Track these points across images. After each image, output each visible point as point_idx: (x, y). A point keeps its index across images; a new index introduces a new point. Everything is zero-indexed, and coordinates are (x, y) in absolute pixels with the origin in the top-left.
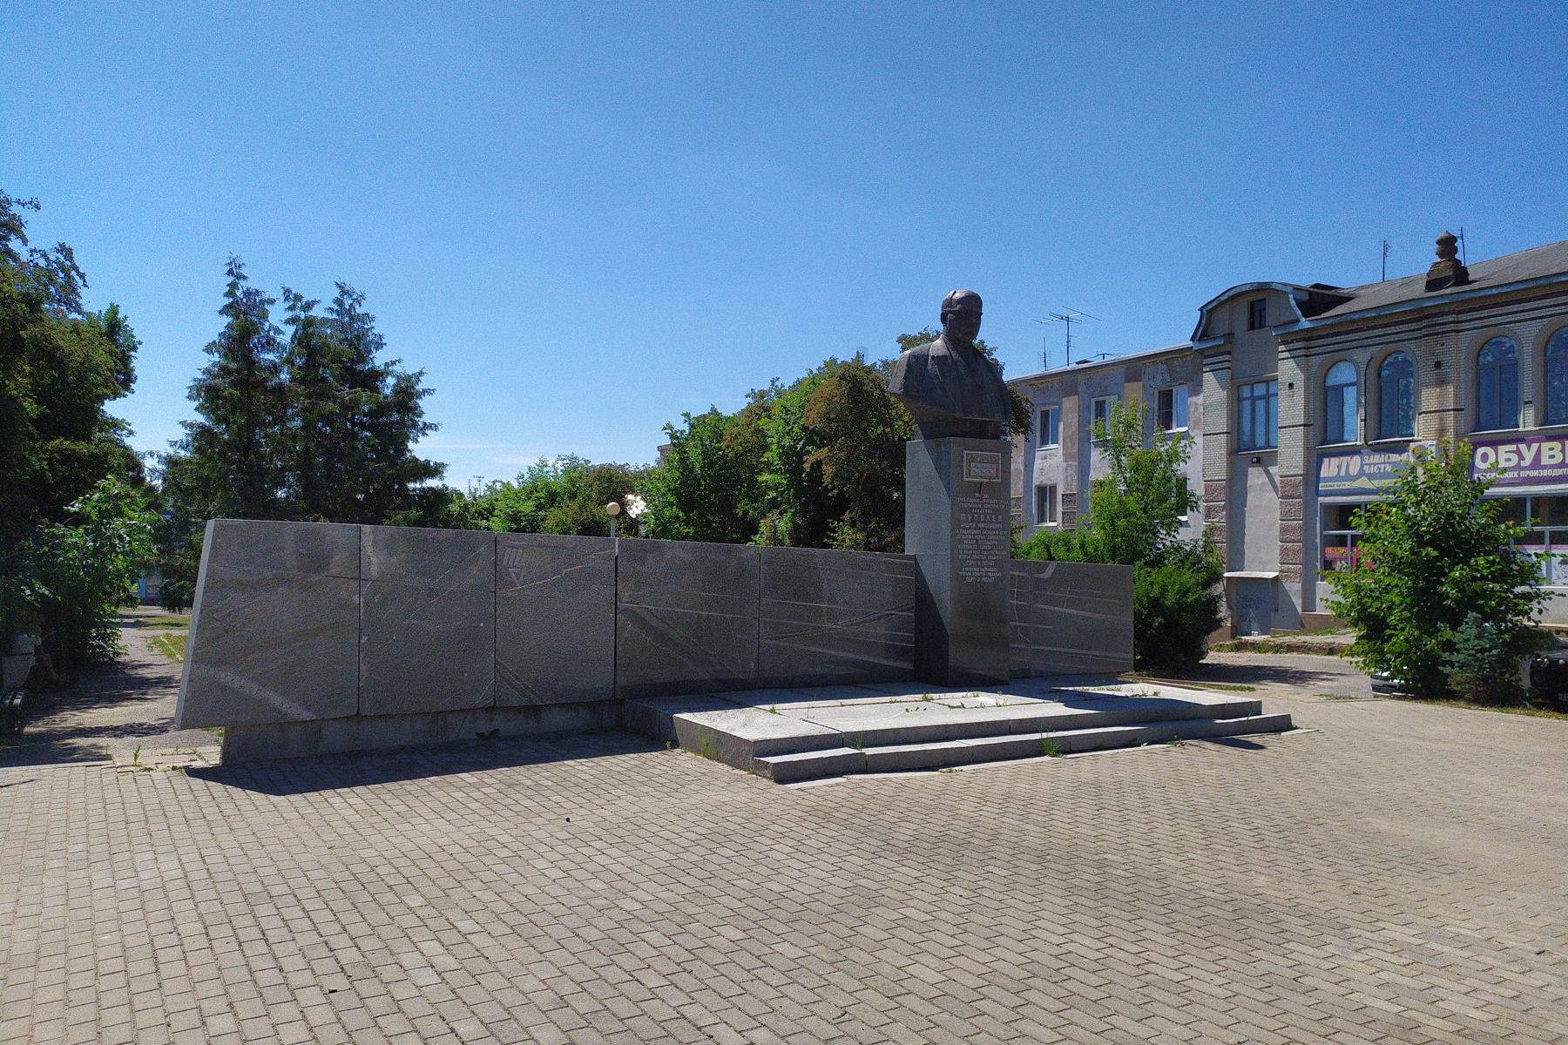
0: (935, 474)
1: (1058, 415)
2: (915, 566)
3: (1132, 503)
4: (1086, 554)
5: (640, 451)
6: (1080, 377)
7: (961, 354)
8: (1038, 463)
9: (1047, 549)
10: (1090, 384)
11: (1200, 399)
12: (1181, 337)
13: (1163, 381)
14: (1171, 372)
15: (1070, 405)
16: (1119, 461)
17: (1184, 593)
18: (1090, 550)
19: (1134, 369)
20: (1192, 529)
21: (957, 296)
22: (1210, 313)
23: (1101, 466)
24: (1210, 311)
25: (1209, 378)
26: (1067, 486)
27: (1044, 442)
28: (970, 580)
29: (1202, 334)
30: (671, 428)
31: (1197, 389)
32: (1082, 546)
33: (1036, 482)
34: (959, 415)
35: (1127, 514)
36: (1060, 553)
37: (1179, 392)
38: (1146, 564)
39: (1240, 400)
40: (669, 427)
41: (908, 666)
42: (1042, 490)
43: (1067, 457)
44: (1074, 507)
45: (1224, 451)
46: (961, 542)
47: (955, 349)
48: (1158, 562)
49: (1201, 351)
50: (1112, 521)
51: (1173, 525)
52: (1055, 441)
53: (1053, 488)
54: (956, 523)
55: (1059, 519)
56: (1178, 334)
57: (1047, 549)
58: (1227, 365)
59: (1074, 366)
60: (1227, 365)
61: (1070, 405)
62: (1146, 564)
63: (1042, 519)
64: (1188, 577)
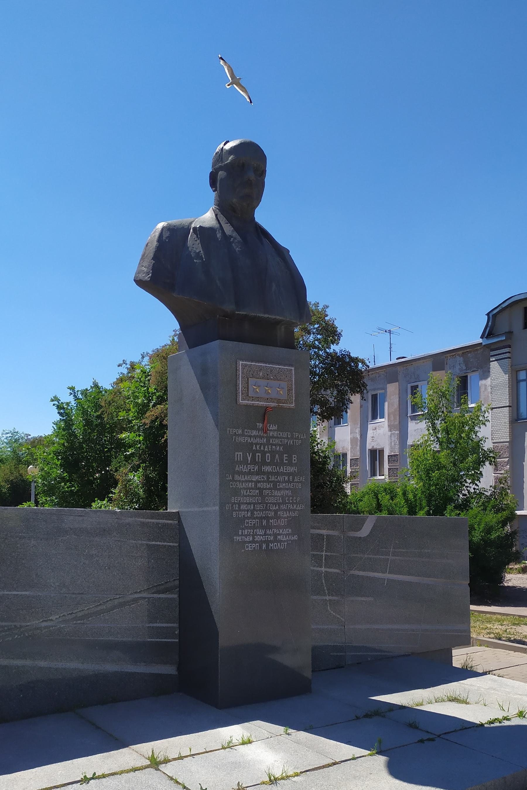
0: (199, 394)
1: (384, 397)
2: (177, 529)
3: (443, 457)
4: (407, 500)
5: (42, 424)
6: (399, 368)
7: (236, 229)
8: (370, 433)
9: (376, 495)
10: (404, 372)
11: (488, 382)
12: (473, 336)
13: (466, 364)
14: (466, 362)
15: (392, 389)
16: (433, 425)
17: (489, 530)
18: (411, 496)
19: (438, 361)
20: (488, 478)
21: (228, 147)
22: (494, 317)
23: (418, 431)
24: (495, 316)
25: (495, 366)
26: (392, 449)
27: (374, 417)
28: (250, 547)
29: (489, 332)
30: (58, 400)
31: (486, 374)
32: (404, 494)
33: (369, 446)
34: (229, 307)
35: (440, 467)
36: (385, 499)
37: (472, 377)
38: (456, 507)
39: (518, 382)
40: (55, 399)
41: (170, 670)
42: (373, 452)
43: (391, 427)
44: (397, 465)
45: (507, 420)
46: (236, 492)
47: (229, 221)
48: (465, 506)
49: (487, 346)
50: (428, 471)
51: (477, 477)
52: (382, 417)
53: (382, 451)
54: (227, 466)
55: (386, 472)
56: (470, 332)
57: (376, 495)
58: (508, 355)
59: (394, 361)
60: (508, 355)
61: (392, 389)
62: (456, 507)
63: (374, 474)
64: (491, 518)
